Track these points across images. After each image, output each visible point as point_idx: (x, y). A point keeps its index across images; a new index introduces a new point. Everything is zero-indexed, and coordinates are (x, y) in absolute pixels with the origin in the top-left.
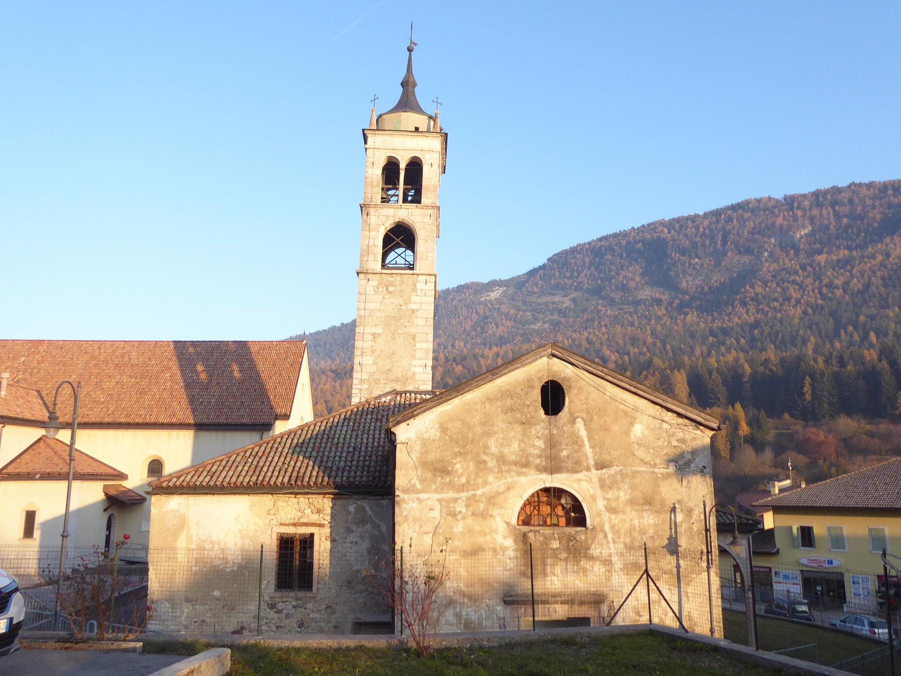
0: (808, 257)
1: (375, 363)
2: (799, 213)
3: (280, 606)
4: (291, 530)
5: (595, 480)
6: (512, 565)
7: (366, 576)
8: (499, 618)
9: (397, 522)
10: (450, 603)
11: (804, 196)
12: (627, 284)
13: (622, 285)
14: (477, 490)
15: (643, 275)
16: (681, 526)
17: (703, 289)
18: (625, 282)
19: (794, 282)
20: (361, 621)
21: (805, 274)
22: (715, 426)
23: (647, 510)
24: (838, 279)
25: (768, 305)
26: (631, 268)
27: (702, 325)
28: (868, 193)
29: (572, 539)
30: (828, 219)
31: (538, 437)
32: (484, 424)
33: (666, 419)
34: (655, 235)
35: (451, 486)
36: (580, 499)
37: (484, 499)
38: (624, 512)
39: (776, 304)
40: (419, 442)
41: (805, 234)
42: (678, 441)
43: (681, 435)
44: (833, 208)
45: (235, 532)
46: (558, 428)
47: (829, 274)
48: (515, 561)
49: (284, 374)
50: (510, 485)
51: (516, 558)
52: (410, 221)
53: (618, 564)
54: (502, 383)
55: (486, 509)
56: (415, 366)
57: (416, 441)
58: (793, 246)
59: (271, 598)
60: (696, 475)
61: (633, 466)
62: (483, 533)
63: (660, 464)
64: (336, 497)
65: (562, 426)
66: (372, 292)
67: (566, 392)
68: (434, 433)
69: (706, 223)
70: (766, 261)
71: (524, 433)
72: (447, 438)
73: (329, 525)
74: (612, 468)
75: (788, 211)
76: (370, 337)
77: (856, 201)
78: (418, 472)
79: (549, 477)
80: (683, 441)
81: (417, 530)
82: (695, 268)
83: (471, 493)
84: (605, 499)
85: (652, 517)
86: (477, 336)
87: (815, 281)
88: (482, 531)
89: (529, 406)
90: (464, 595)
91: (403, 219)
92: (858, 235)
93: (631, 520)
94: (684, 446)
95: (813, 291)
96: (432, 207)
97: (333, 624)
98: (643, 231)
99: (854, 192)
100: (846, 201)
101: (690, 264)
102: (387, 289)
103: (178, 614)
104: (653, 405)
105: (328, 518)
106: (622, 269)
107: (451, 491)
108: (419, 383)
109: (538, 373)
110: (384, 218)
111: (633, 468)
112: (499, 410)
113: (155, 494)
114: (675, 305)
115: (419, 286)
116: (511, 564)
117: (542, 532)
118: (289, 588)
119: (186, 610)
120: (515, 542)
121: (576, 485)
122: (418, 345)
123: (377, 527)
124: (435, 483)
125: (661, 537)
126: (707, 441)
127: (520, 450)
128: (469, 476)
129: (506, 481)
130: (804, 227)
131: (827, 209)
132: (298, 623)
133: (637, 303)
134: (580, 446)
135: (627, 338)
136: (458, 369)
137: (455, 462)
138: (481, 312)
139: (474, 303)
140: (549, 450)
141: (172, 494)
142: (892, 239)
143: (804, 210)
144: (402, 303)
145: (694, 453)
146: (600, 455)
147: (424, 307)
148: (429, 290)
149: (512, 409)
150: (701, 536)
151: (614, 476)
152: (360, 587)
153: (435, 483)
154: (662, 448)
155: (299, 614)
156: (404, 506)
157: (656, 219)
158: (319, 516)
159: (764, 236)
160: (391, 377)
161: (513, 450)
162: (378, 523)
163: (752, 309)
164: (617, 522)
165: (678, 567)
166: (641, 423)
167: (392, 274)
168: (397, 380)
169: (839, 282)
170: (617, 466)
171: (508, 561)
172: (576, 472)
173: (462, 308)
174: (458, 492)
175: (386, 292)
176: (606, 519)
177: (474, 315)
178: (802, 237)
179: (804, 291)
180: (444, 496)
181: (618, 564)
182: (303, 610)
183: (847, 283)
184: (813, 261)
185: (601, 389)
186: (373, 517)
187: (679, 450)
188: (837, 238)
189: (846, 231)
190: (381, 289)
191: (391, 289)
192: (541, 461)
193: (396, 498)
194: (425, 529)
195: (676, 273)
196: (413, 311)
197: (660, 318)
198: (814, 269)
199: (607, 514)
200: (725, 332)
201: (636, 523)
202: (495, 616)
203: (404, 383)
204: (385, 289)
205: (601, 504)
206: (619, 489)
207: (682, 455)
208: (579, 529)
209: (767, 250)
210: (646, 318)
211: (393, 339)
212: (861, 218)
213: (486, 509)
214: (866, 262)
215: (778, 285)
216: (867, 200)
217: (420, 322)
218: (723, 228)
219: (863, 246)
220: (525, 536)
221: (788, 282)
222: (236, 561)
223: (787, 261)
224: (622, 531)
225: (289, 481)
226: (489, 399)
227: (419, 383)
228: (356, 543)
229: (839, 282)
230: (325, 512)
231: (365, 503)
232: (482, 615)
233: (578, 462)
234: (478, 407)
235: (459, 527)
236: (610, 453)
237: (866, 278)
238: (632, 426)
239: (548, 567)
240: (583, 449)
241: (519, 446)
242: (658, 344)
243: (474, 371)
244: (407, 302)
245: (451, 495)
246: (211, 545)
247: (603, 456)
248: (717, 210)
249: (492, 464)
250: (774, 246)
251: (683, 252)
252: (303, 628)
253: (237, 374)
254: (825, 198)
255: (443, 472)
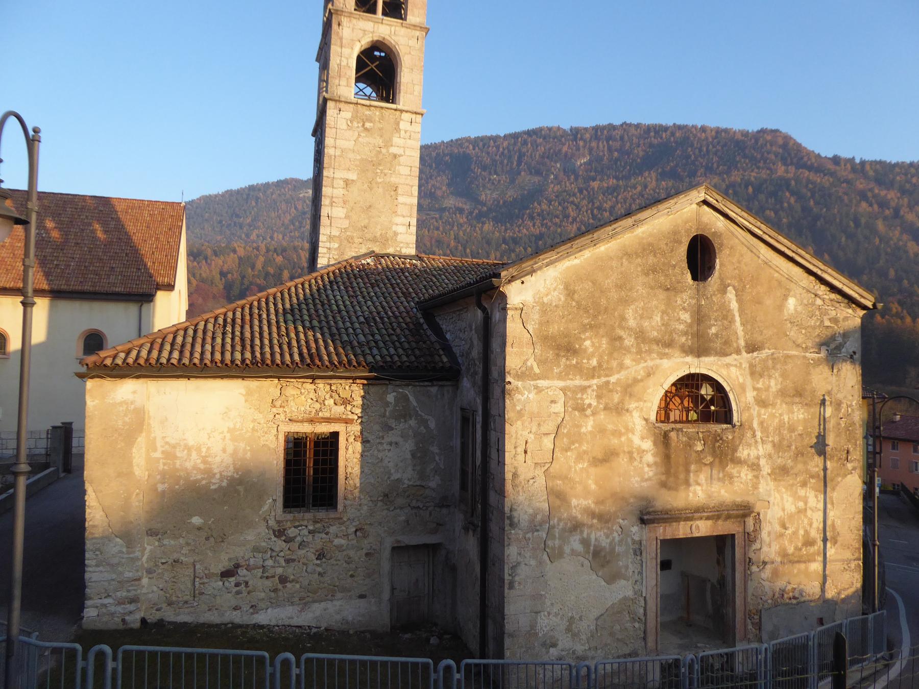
0: (585, 182)
1: (347, 217)
2: (581, 143)
3: (292, 532)
4: (305, 428)
5: (745, 365)
6: (651, 474)
7: (409, 486)
8: (634, 542)
9: (508, 419)
10: (576, 527)
11: (586, 129)
12: (434, 192)
13: (431, 192)
14: (611, 376)
15: (449, 185)
16: (829, 422)
17: (499, 202)
18: (433, 190)
19: (572, 203)
20: (402, 545)
21: (582, 196)
22: (869, 304)
23: (797, 403)
24: (606, 202)
25: (551, 221)
26: (439, 178)
27: (497, 234)
28: (635, 133)
29: (718, 438)
30: (603, 151)
31: (684, 309)
32: (620, 287)
33: (820, 293)
34: (461, 150)
35: (578, 370)
36: (727, 389)
37: (619, 389)
38: (773, 405)
39: (557, 220)
40: (538, 308)
41: (585, 163)
42: (830, 319)
43: (833, 313)
44: (608, 142)
45: (222, 433)
46: (707, 298)
47: (600, 198)
48: (654, 468)
49: (162, 238)
50: (650, 369)
51: (655, 463)
52: (392, 42)
53: (766, 469)
54: (643, 233)
55: (622, 402)
56: (397, 225)
57: (533, 306)
58: (574, 172)
59: (278, 522)
60: (846, 361)
61: (784, 350)
62: (617, 433)
63: (812, 348)
64: (370, 382)
65: (711, 296)
66: (344, 127)
67: (717, 251)
68: (557, 296)
69: (505, 144)
70: (552, 182)
71: (669, 303)
72: (574, 304)
73: (359, 421)
74: (764, 352)
75: (572, 141)
76: (342, 183)
77: (626, 137)
78: (536, 351)
79: (696, 360)
80: (835, 320)
81: (534, 430)
82: (493, 183)
83: (604, 379)
84: (755, 389)
85: (802, 411)
86: (295, 230)
87: (589, 203)
88: (616, 431)
89: (674, 266)
90: (593, 515)
91: (384, 38)
92: (624, 168)
93: (781, 415)
94: (836, 327)
95: (587, 212)
96: (421, 27)
97: (364, 551)
98: (451, 146)
99: (625, 130)
100: (618, 137)
101: (490, 179)
102: (363, 125)
103: (138, 554)
104: (806, 275)
105: (358, 411)
106: (431, 178)
107: (578, 377)
108: (402, 245)
109: (686, 223)
110: (361, 34)
111: (785, 352)
112: (639, 269)
113: (92, 378)
114: (474, 214)
115: (403, 125)
116: (649, 472)
117: (685, 430)
118: (303, 506)
119: (149, 548)
120: (655, 443)
121: (724, 372)
122: (401, 199)
123: (423, 422)
124: (559, 366)
125: (809, 434)
126: (858, 321)
127: (663, 325)
128: (601, 357)
129: (645, 365)
130: (584, 156)
131: (603, 143)
132: (317, 553)
133: (443, 210)
134: (730, 322)
135: (433, 240)
136: (279, 259)
137: (583, 337)
138: (300, 207)
139: (293, 199)
140: (696, 325)
141: (122, 377)
142: (650, 174)
143: (585, 141)
144: (382, 145)
145: (845, 335)
146: (752, 334)
147: (408, 152)
148: (415, 132)
149: (654, 270)
150: (848, 432)
151: (765, 361)
152: (400, 501)
153: (559, 366)
154: (814, 328)
155: (318, 541)
156: (518, 396)
157: (464, 136)
158: (345, 408)
159: (552, 161)
160: (368, 236)
161: (654, 324)
162: (426, 417)
163: (538, 223)
164: (766, 417)
165: (825, 469)
166: (795, 297)
167: (370, 106)
168: (374, 240)
169: (607, 206)
170: (769, 349)
171: (646, 469)
172: (725, 355)
173: (281, 202)
174: (587, 379)
175: (362, 129)
176: (755, 413)
177: (293, 210)
178: (581, 165)
179: (580, 211)
180: (569, 383)
181: (766, 469)
182: (324, 536)
183: (612, 208)
184: (589, 186)
185: (754, 251)
186: (418, 409)
187: (830, 330)
188: (608, 169)
189: (616, 164)
190: (355, 124)
191: (368, 125)
192: (687, 340)
193: (507, 387)
194: (544, 429)
195: (478, 186)
196: (395, 156)
197: (462, 225)
198: (589, 193)
199: (757, 408)
200: (515, 241)
201: (786, 418)
202: (629, 540)
203: (384, 244)
204: (360, 125)
205: (750, 395)
206: (770, 377)
207: (833, 338)
208: (725, 426)
209: (553, 173)
210: (450, 225)
211: (371, 189)
212: (628, 153)
213: (622, 402)
214: (629, 192)
215: (560, 204)
216: (634, 138)
217: (404, 171)
218: (520, 150)
219: (627, 178)
220: (666, 435)
221: (568, 203)
222: (225, 474)
223: (568, 184)
224: (771, 428)
225: (202, 359)
226: (627, 254)
227: (402, 245)
228: (396, 443)
229: (607, 206)
230: (354, 403)
231: (408, 391)
232: (614, 539)
233: (727, 343)
234: (614, 264)
235: (588, 426)
236: (761, 332)
237: (628, 204)
238: (786, 300)
239: (692, 475)
240: (733, 327)
241: (662, 319)
242: (460, 248)
243: (294, 263)
244: (388, 143)
245: (578, 382)
246: (186, 452)
247: (755, 336)
248: (515, 133)
249: (629, 341)
250: (559, 170)
251: (484, 168)
252: (324, 560)
253: (100, 234)
254: (602, 133)
255: (568, 351)
